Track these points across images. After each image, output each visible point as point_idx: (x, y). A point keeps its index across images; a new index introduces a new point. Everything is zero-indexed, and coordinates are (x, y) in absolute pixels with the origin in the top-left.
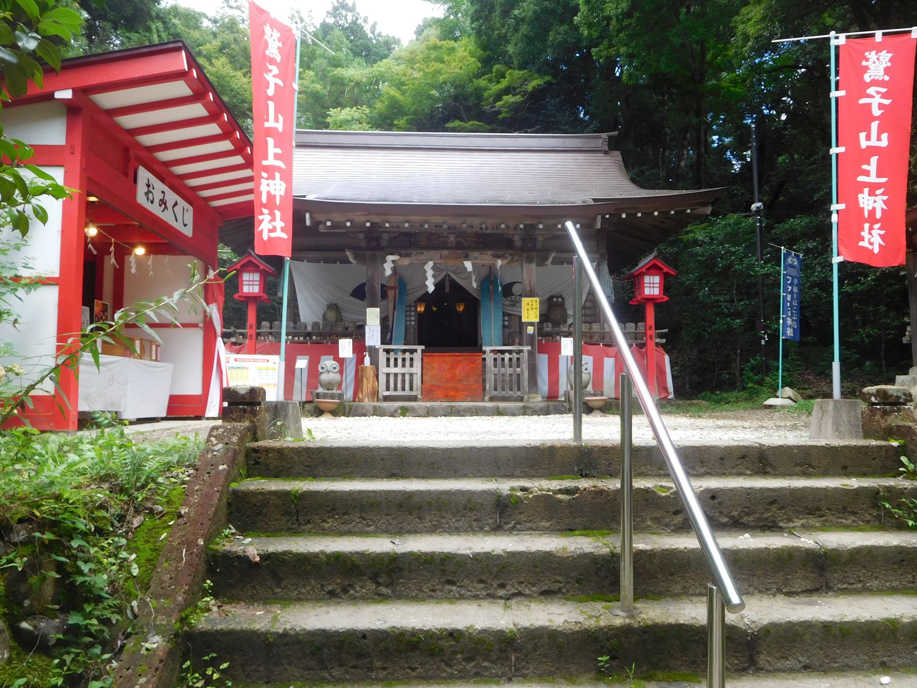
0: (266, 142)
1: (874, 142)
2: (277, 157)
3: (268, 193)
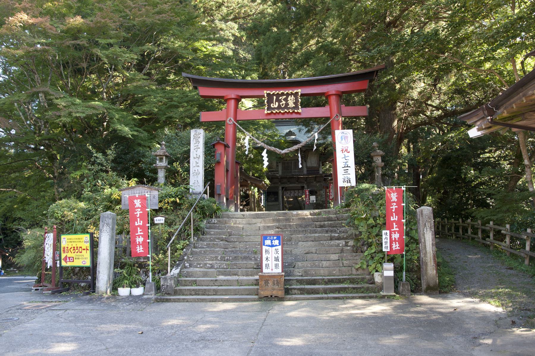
1: (139, 224)
2: (140, 232)
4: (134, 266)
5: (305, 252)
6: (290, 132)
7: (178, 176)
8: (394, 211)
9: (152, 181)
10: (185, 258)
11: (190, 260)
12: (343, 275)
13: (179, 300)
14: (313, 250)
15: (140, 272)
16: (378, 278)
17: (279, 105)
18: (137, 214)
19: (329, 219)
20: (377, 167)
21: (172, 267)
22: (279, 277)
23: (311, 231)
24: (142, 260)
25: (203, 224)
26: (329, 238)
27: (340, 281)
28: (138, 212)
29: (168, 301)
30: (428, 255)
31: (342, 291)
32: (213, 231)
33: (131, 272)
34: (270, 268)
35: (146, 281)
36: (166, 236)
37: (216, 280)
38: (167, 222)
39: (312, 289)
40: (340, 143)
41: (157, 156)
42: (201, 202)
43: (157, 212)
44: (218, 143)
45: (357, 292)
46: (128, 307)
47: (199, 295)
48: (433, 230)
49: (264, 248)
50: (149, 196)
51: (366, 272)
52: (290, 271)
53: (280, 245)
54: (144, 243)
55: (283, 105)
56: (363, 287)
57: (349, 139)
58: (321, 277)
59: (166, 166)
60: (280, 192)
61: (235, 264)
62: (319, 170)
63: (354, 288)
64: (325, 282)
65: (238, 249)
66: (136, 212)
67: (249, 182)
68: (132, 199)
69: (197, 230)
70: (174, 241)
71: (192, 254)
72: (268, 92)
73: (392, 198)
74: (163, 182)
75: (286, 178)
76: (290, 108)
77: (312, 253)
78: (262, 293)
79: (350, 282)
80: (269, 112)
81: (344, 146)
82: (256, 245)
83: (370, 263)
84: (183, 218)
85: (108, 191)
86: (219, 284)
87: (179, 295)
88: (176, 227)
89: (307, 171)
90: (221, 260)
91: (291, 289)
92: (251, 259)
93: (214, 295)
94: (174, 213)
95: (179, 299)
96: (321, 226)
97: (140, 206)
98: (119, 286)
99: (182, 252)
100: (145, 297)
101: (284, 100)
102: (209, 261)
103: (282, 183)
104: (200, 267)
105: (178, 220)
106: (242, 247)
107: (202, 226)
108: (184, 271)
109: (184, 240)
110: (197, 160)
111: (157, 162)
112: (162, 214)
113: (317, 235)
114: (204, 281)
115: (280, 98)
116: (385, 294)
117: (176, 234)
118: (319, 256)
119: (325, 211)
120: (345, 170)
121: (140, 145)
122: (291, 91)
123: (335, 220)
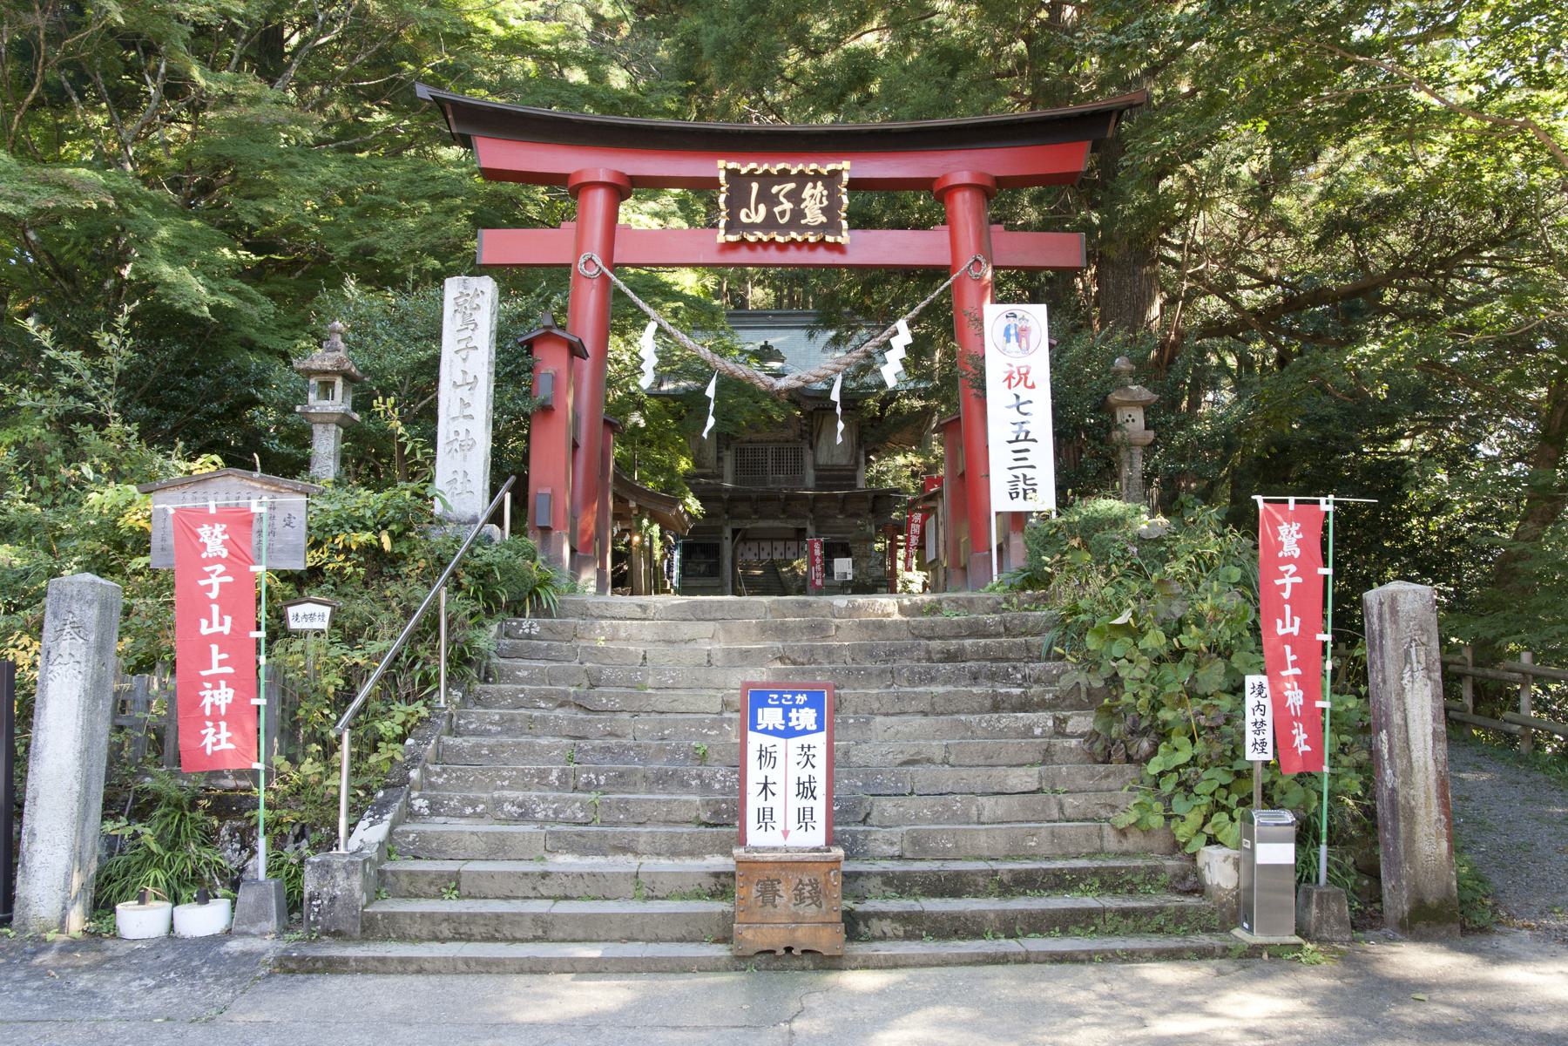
0: (210, 650)
1: (216, 628)
2: (222, 663)
3: (213, 705)
4: (193, 806)
5: (901, 758)
6: (766, 347)
7: (387, 451)
8: (1286, 595)
9: (288, 465)
10: (414, 774)
11: (432, 786)
12: (1065, 856)
13: (381, 967)
14: (936, 748)
15: (217, 832)
16: (1218, 869)
17: (770, 215)
18: (209, 588)
19: (976, 631)
20: (1130, 446)
21: (356, 811)
22: (825, 868)
23: (912, 672)
24: (230, 783)
25: (488, 637)
26: (988, 703)
27: (1060, 882)
28: (216, 580)
29: (333, 966)
30: (1419, 778)
31: (1076, 923)
32: (524, 668)
33: (178, 834)
34: (779, 826)
35: (242, 870)
36: (332, 682)
37: (545, 875)
38: (342, 627)
39: (954, 917)
40: (1003, 351)
41: (309, 373)
42: (479, 550)
43: (302, 582)
44: (547, 336)
45: (1137, 931)
46: (151, 1002)
47: (469, 938)
48: (1437, 675)
49: (755, 740)
50: (264, 510)
51: (1159, 843)
52: (854, 835)
53: (820, 729)
54: (233, 716)
55: (782, 214)
56: (1161, 909)
57: (1033, 338)
58: (981, 866)
59: (345, 415)
60: (727, 546)
61: (624, 806)
62: (854, 478)
63: (1125, 913)
64: (1001, 883)
65: (628, 741)
66: (207, 576)
67: (633, 504)
68: (189, 522)
69: (462, 659)
70: (366, 702)
71: (439, 757)
72: (732, 165)
73: (1280, 545)
74: (331, 477)
75: (748, 499)
76: (807, 227)
77: (930, 761)
78: (749, 935)
79: (1103, 884)
80: (732, 238)
81: (1016, 363)
82: (701, 724)
83: (1179, 805)
84: (408, 613)
85: (102, 498)
86: (558, 892)
87: (385, 938)
88: (375, 647)
89: (818, 478)
90: (563, 784)
91: (866, 917)
92: (684, 785)
93: (536, 939)
94: (372, 593)
95: (383, 960)
96: (950, 657)
97: (225, 554)
98: (123, 895)
99: (398, 752)
100: (235, 946)
101: (788, 196)
102: (510, 787)
103: (733, 517)
104: (475, 815)
105: (385, 618)
106: (645, 733)
107: (481, 644)
108: (407, 834)
109: (410, 699)
110: (464, 392)
111: (312, 396)
112: (322, 593)
113: (938, 689)
114: (491, 875)
115: (775, 190)
116: (1258, 938)
117: (374, 675)
118: (964, 773)
119: (955, 601)
120: (1018, 454)
121: (250, 345)
122: (813, 166)
123: (998, 635)
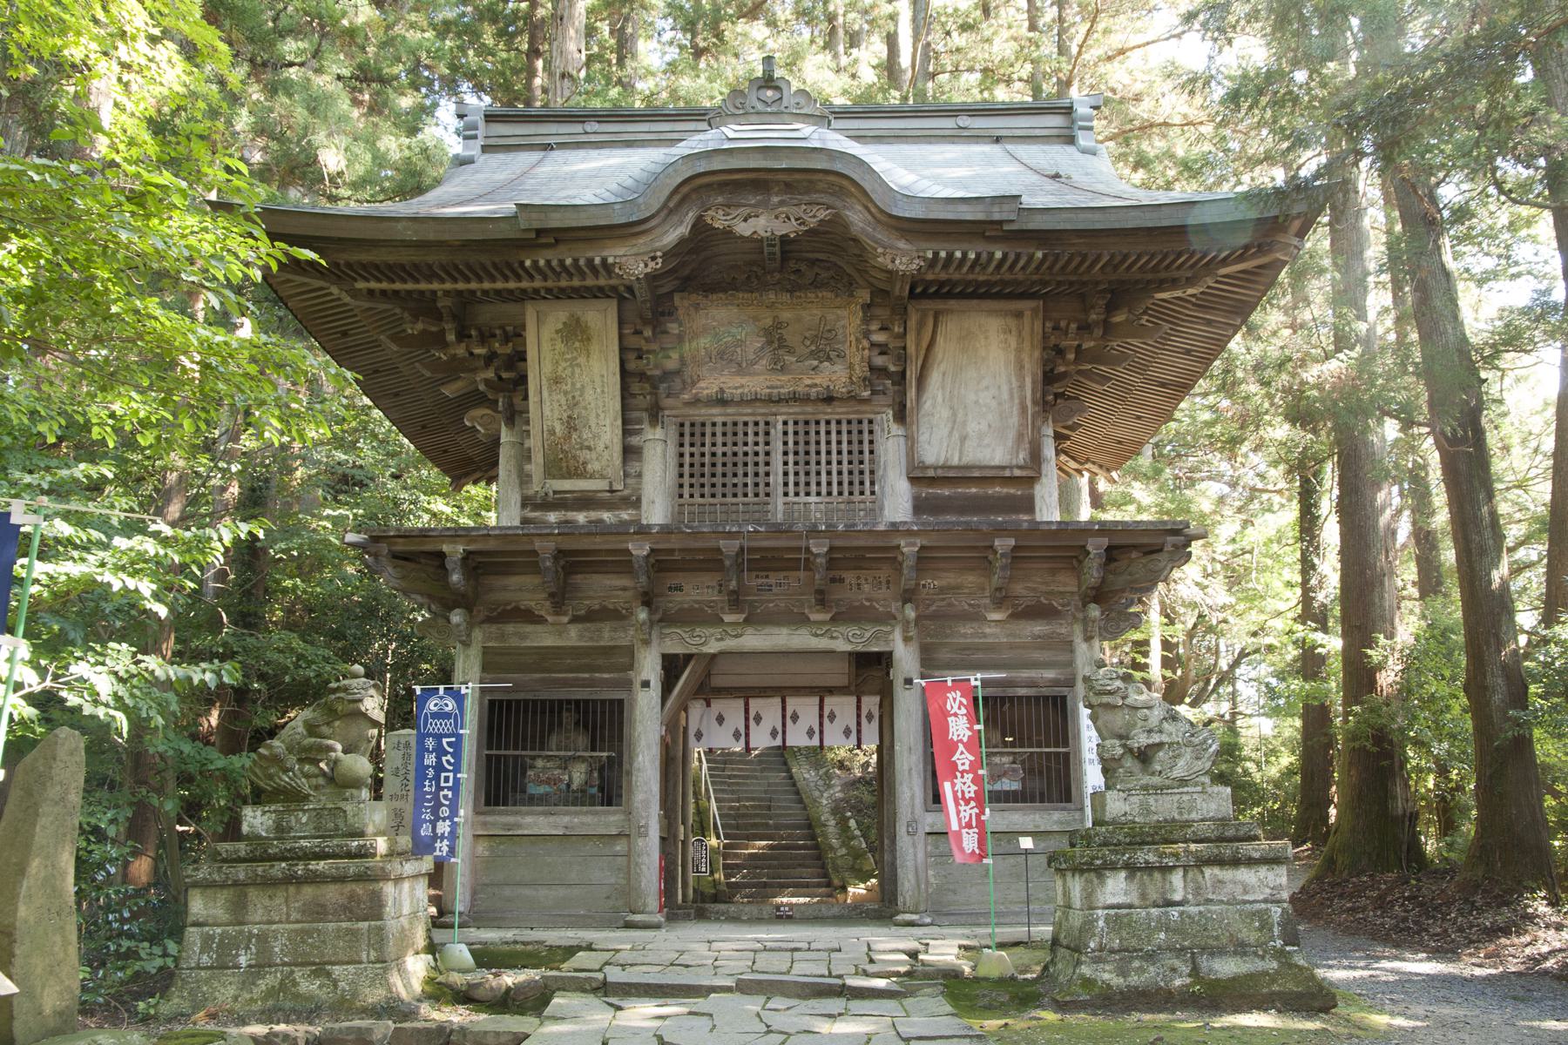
63: (383, 292)
75: (710, 562)
103: (668, 619)
